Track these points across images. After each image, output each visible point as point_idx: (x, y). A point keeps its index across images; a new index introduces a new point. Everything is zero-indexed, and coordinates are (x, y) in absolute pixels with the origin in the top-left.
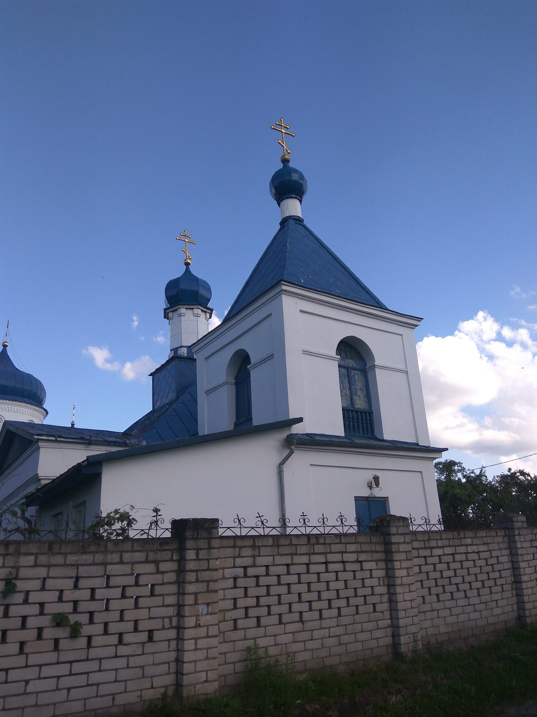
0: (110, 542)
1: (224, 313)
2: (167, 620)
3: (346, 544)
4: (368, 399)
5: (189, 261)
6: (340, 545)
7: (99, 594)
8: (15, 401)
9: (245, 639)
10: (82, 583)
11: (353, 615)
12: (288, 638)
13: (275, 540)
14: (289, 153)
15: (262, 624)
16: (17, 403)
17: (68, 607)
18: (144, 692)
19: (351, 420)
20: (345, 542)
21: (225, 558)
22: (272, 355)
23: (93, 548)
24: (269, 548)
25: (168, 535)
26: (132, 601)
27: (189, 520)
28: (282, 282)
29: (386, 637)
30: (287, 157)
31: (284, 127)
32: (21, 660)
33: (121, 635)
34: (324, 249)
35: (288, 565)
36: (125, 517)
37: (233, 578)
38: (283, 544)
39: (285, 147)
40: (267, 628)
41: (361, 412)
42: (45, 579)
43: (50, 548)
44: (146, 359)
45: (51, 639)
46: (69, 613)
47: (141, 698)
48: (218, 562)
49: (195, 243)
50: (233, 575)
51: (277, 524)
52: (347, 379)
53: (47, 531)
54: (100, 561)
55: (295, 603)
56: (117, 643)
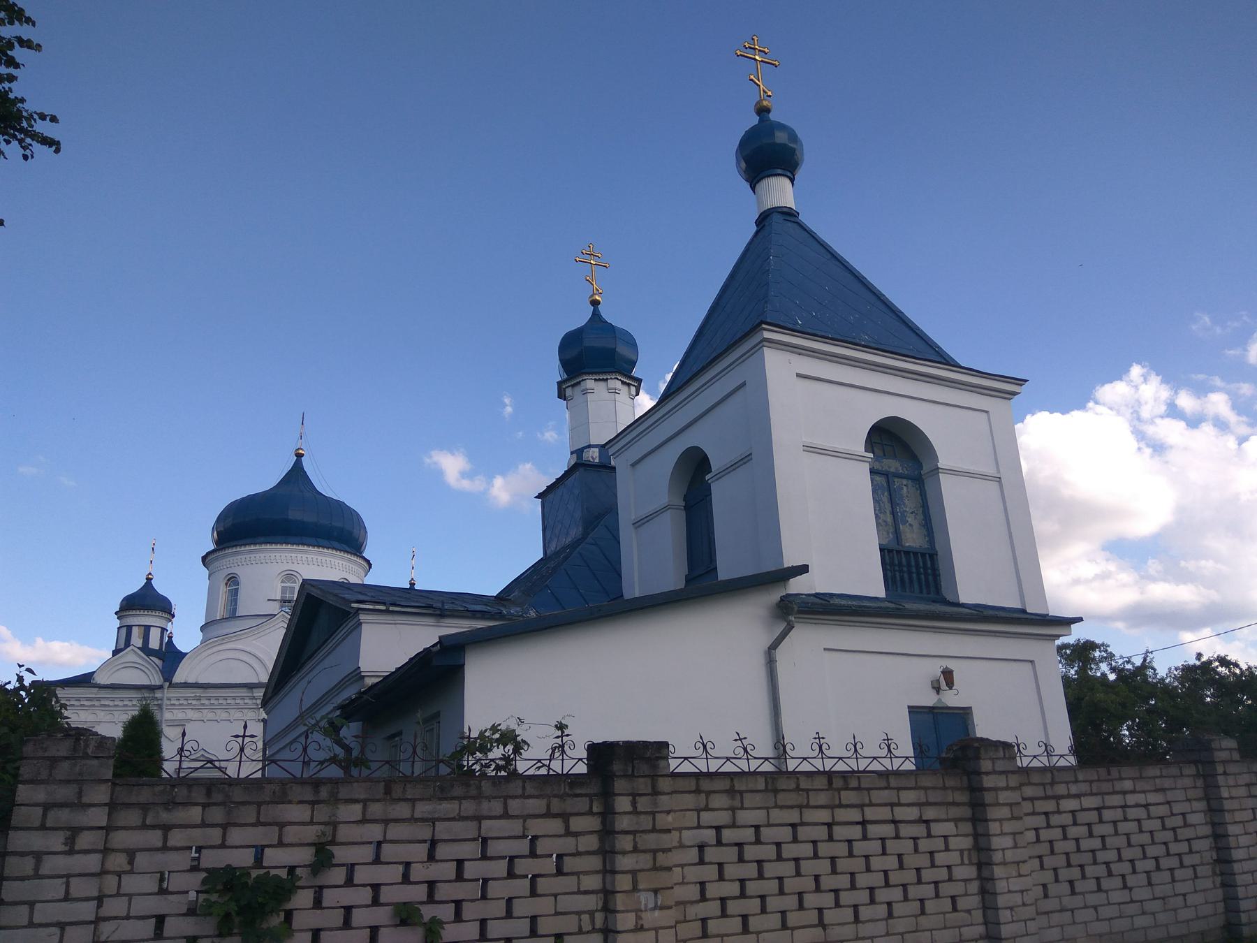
1: (657, 386)
2: (585, 918)
3: (899, 789)
5: (597, 298)
7: (470, 870)
10: (442, 851)
11: (916, 916)
14: (770, 96)
16: (321, 549)
17: (419, 893)
19: (905, 569)
21: (682, 810)
23: (458, 791)
24: (760, 794)
25: (582, 769)
26: (527, 882)
27: (617, 743)
28: (764, 326)
30: (765, 103)
31: (760, 50)
35: (794, 826)
36: (508, 737)
38: (784, 787)
39: (762, 87)
42: (379, 843)
43: (388, 791)
48: (670, 818)
51: (768, 751)
52: (886, 494)
53: (801, 758)
54: (470, 813)
55: (810, 892)
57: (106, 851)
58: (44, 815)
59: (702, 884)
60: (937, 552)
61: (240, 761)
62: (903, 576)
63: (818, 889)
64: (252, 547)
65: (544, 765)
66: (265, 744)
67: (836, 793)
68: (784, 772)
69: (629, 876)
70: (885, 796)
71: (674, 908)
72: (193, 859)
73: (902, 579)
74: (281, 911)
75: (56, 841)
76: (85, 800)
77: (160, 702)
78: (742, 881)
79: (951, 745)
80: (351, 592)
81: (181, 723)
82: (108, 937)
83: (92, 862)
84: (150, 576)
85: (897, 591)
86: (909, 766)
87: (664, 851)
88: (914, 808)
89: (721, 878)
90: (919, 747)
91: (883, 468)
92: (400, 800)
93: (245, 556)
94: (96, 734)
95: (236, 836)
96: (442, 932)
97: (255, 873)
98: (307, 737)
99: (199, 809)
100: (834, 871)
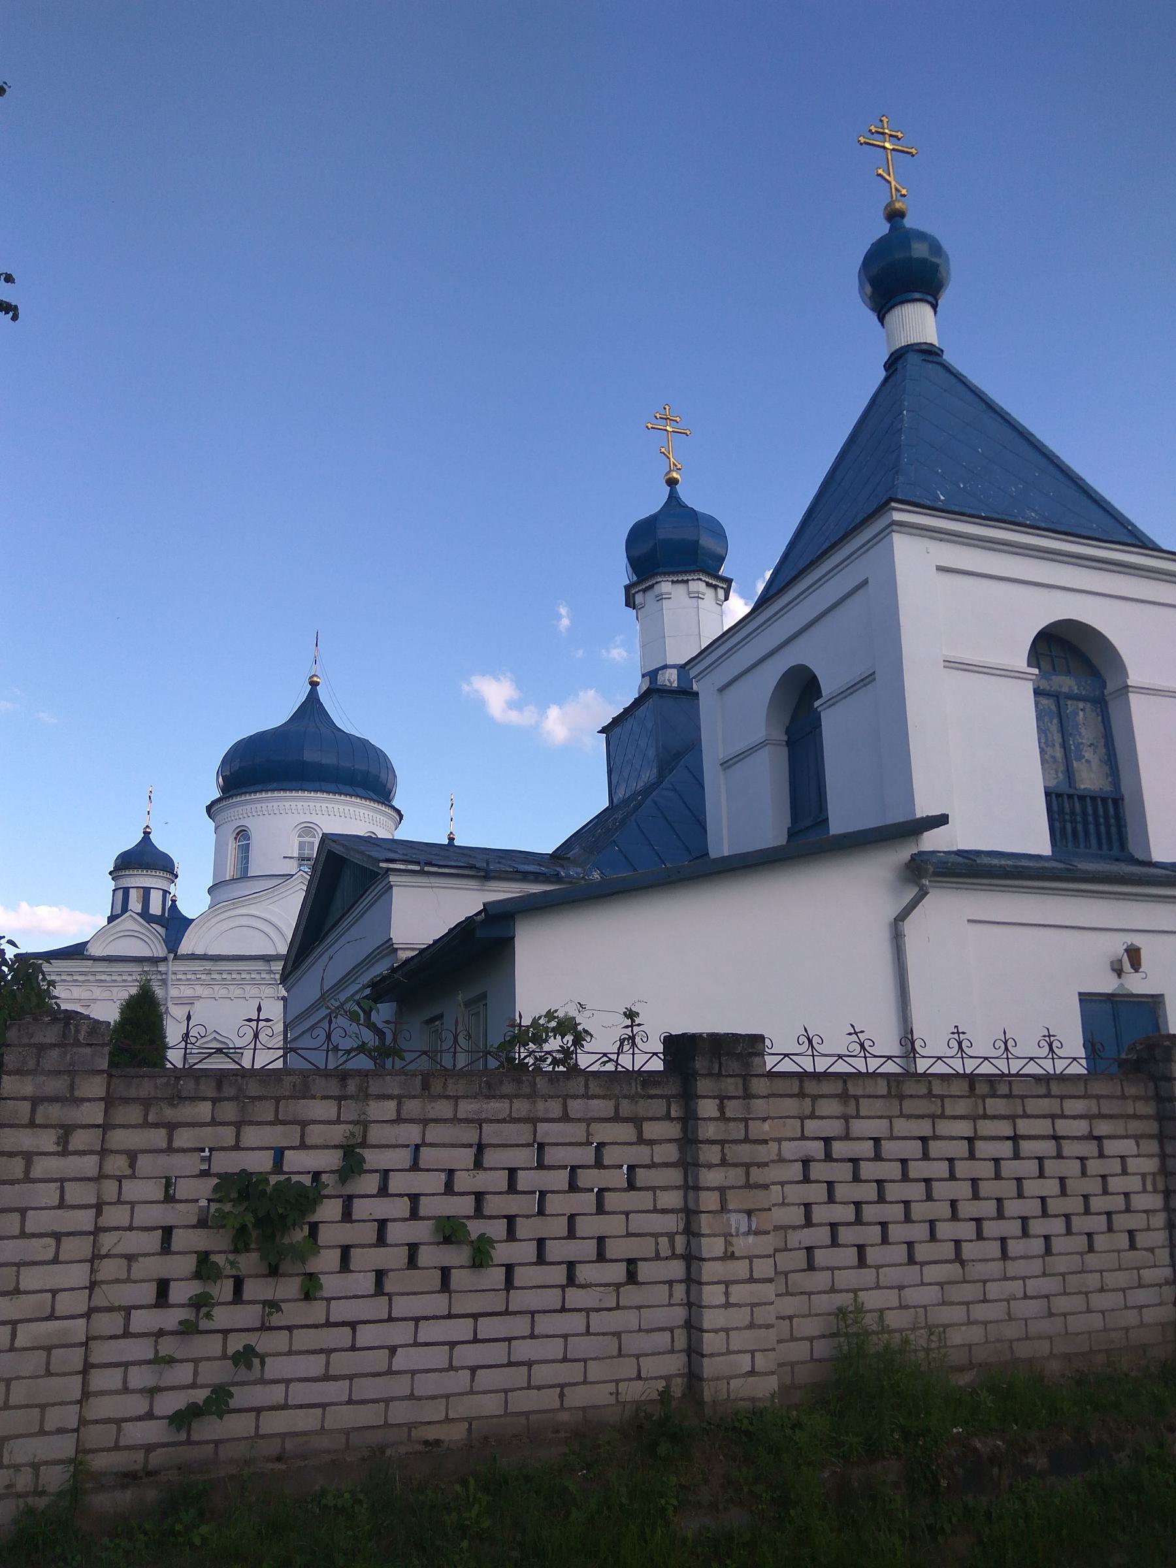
0: (541, 1077)
1: (755, 587)
2: (663, 1241)
3: (1062, 1097)
4: (1111, 768)
5: (675, 475)
6: (1046, 1100)
7: (525, 1180)
8: (340, 794)
9: (833, 1290)
10: (490, 1157)
11: (1082, 1254)
12: (930, 1294)
13: (894, 1085)
14: (904, 196)
15: (869, 1261)
16: (343, 797)
17: (464, 1206)
18: (622, 1386)
19: (1067, 817)
20: (1058, 1093)
21: (781, 1118)
22: (871, 675)
23: (507, 1088)
24: (880, 1100)
25: (657, 1065)
26: (592, 1197)
27: (701, 1035)
28: (893, 504)
29: (1160, 1304)
30: (898, 205)
31: (891, 136)
32: (378, 1308)
33: (571, 1266)
34: (995, 416)
35: (924, 1140)
36: (566, 1026)
37: (802, 1161)
38: (913, 1093)
39: (893, 183)
40: (880, 1270)
41: (1093, 799)
42: (417, 1147)
43: (426, 1086)
44: (589, 696)
45: (435, 1268)
46: (468, 1217)
47: (617, 1398)
48: (766, 1126)
49: (688, 433)
50: (801, 1156)
51: (894, 1049)
52: (1055, 721)
54: (523, 1114)
55: (944, 1220)
56: (564, 1282)
57: (103, 1153)
58: (33, 1111)
59: (807, 1206)
60: (1123, 796)
61: (255, 1049)
62: (1076, 827)
63: (955, 1217)
64: (264, 795)
65: (610, 1060)
66: (286, 1027)
67: (980, 1101)
68: (913, 1073)
69: (716, 1194)
70: (1044, 1105)
71: (772, 1233)
72: (203, 1159)
74: (304, 1223)
75: (47, 1141)
76: (77, 1094)
77: (164, 977)
78: (858, 1205)
79: (1134, 1044)
80: (378, 848)
81: (190, 1001)
82: (109, 1250)
83: (89, 1165)
84: (147, 830)
85: (1067, 847)
86: (1078, 1069)
87: (760, 1165)
88: (1083, 1121)
89: (831, 1199)
90: (1091, 1045)
91: (1051, 687)
92: (440, 1097)
93: (272, 804)
94: (88, 1017)
95: (252, 1136)
96: (493, 1252)
97: (273, 1180)
98: (330, 1022)
99: (209, 1104)
100: (976, 1196)
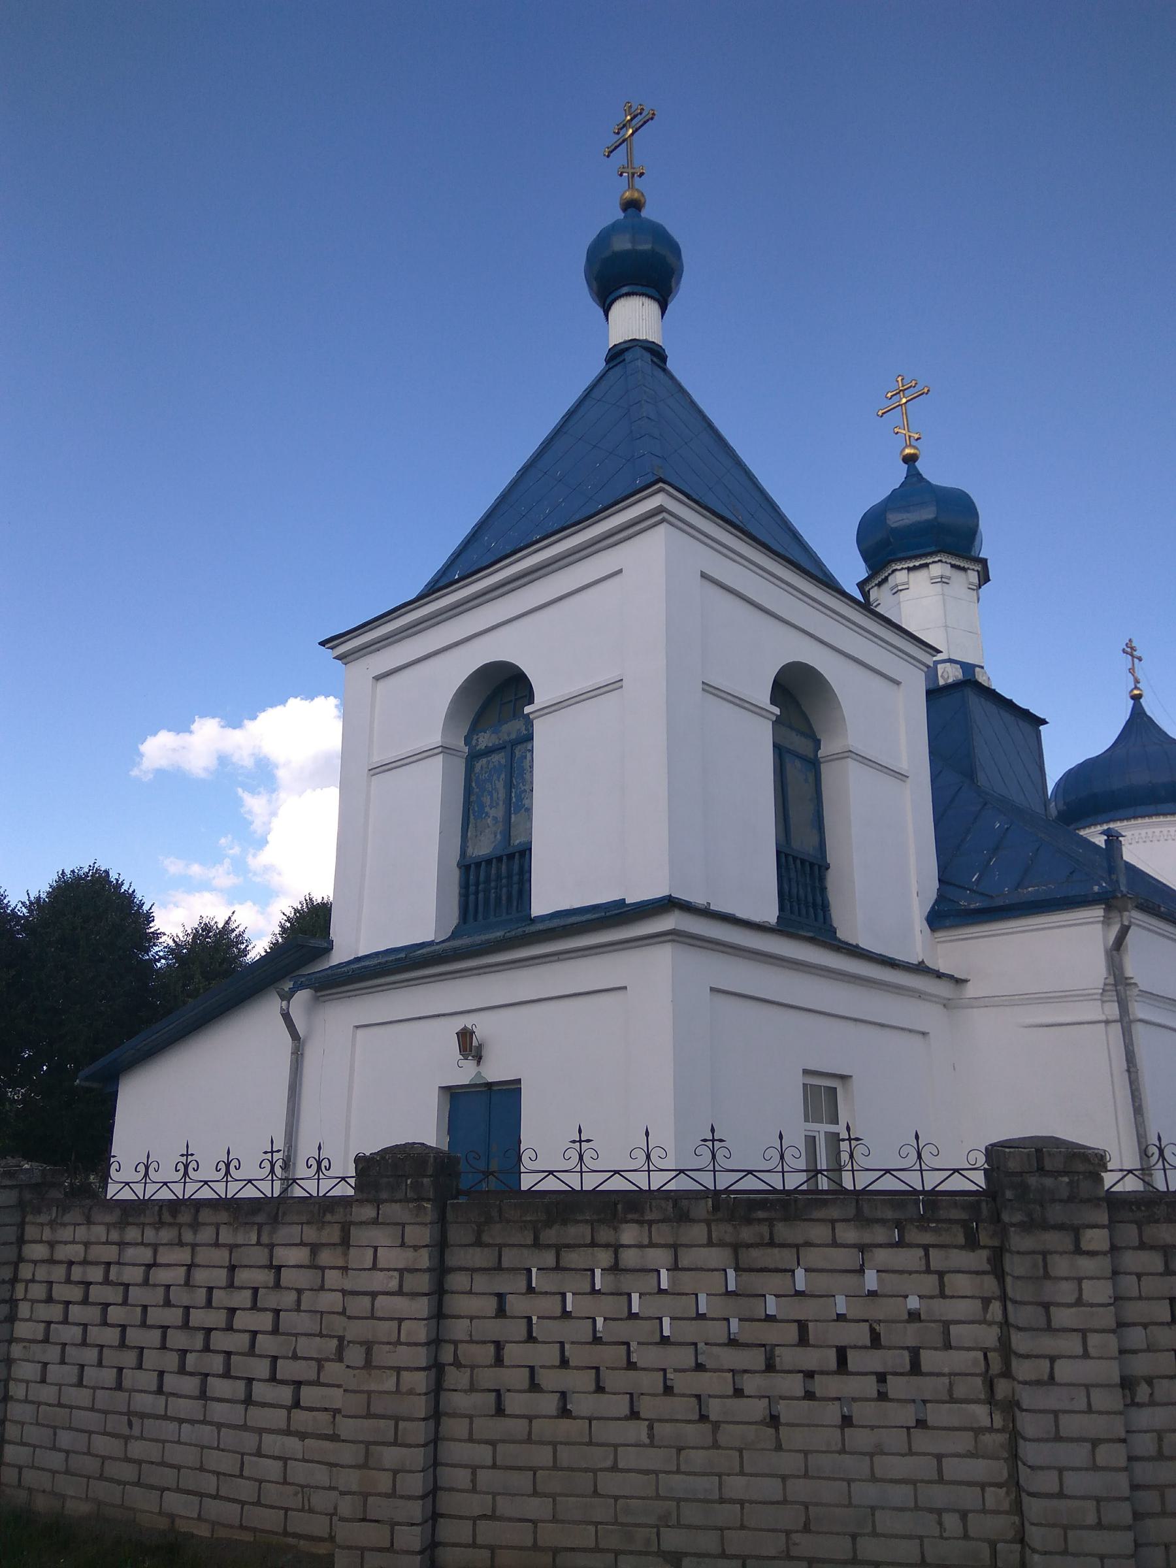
16: (1140, 821)
53: (245, 1180)
73: (498, 899)
